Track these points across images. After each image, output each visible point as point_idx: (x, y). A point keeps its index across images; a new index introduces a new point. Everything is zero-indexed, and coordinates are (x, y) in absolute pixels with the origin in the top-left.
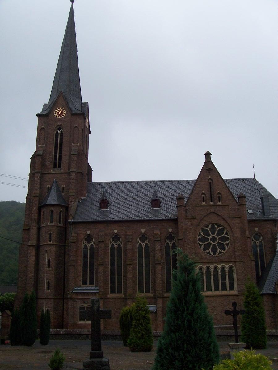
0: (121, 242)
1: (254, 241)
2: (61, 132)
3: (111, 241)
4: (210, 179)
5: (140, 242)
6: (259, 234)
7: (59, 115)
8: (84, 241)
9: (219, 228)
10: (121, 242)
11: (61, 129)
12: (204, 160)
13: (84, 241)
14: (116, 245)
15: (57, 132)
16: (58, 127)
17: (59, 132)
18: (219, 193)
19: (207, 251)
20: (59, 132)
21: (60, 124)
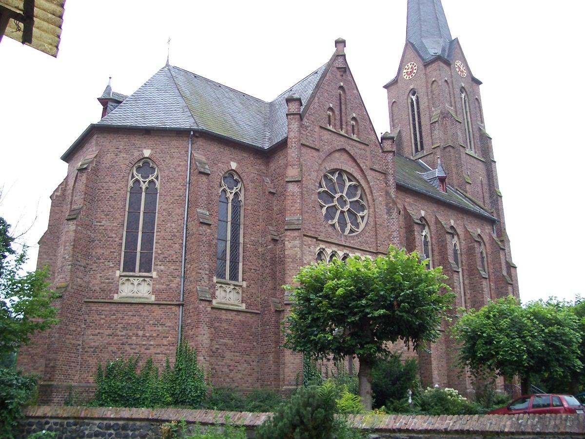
0: (157, 178)
1: (137, 177)
2: (417, 97)
3: (133, 174)
4: (341, 88)
5: (138, 177)
6: (236, 177)
7: (409, 74)
8: (135, 172)
9: (351, 183)
10: (157, 178)
11: (416, 93)
12: (332, 50)
13: (135, 172)
14: (144, 182)
15: (412, 100)
16: (412, 92)
17: (414, 98)
18: (354, 119)
19: (330, 222)
20: (414, 98)
21: (412, 87)
